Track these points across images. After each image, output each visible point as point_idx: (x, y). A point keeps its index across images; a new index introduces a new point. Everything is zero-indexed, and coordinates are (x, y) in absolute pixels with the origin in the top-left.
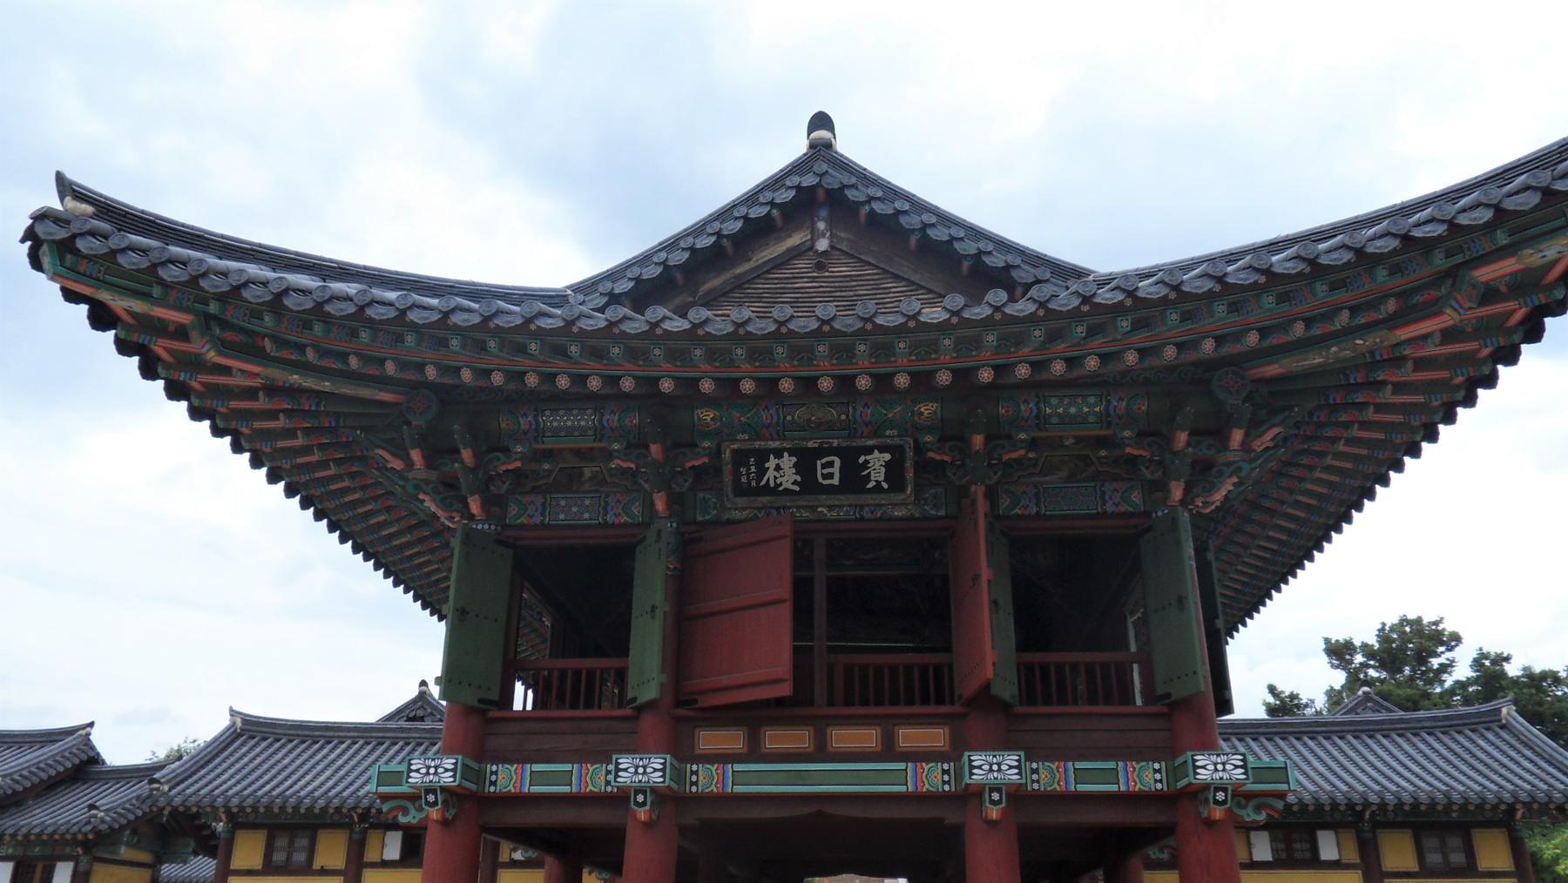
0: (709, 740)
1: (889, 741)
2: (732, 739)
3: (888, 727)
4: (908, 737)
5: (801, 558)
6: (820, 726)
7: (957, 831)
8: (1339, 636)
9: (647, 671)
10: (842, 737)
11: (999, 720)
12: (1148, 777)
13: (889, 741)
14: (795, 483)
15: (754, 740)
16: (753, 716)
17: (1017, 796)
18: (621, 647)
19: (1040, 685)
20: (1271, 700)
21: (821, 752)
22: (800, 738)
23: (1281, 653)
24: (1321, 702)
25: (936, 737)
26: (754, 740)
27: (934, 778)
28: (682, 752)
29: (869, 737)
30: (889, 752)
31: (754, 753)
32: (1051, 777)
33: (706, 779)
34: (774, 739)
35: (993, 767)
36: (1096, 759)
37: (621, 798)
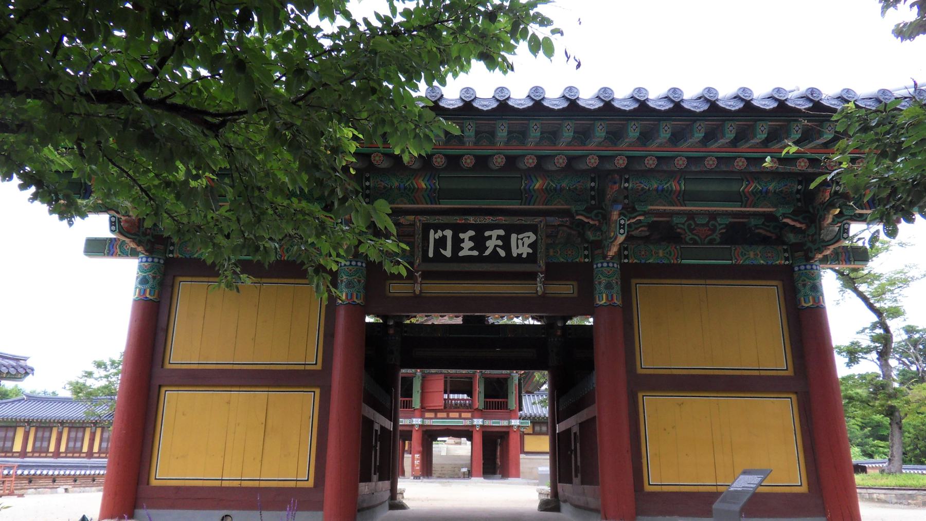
0: (427, 415)
1: (460, 416)
2: (432, 415)
3: (460, 412)
4: (464, 415)
5: (445, 382)
6: (448, 412)
8: (98, 359)
9: (416, 402)
10: (451, 415)
11: (481, 413)
12: (505, 423)
13: (460, 416)
16: (436, 411)
17: (482, 426)
18: (506, 396)
19: (487, 406)
21: (448, 418)
22: (444, 415)
23: (317, 8)
24: (474, 62)
27: (468, 423)
28: (422, 417)
29: (457, 415)
30: (460, 418)
31: (436, 418)
32: (488, 423)
33: (428, 422)
34: (439, 415)
35: (478, 422)
36: (694, 265)
37: (413, 425)
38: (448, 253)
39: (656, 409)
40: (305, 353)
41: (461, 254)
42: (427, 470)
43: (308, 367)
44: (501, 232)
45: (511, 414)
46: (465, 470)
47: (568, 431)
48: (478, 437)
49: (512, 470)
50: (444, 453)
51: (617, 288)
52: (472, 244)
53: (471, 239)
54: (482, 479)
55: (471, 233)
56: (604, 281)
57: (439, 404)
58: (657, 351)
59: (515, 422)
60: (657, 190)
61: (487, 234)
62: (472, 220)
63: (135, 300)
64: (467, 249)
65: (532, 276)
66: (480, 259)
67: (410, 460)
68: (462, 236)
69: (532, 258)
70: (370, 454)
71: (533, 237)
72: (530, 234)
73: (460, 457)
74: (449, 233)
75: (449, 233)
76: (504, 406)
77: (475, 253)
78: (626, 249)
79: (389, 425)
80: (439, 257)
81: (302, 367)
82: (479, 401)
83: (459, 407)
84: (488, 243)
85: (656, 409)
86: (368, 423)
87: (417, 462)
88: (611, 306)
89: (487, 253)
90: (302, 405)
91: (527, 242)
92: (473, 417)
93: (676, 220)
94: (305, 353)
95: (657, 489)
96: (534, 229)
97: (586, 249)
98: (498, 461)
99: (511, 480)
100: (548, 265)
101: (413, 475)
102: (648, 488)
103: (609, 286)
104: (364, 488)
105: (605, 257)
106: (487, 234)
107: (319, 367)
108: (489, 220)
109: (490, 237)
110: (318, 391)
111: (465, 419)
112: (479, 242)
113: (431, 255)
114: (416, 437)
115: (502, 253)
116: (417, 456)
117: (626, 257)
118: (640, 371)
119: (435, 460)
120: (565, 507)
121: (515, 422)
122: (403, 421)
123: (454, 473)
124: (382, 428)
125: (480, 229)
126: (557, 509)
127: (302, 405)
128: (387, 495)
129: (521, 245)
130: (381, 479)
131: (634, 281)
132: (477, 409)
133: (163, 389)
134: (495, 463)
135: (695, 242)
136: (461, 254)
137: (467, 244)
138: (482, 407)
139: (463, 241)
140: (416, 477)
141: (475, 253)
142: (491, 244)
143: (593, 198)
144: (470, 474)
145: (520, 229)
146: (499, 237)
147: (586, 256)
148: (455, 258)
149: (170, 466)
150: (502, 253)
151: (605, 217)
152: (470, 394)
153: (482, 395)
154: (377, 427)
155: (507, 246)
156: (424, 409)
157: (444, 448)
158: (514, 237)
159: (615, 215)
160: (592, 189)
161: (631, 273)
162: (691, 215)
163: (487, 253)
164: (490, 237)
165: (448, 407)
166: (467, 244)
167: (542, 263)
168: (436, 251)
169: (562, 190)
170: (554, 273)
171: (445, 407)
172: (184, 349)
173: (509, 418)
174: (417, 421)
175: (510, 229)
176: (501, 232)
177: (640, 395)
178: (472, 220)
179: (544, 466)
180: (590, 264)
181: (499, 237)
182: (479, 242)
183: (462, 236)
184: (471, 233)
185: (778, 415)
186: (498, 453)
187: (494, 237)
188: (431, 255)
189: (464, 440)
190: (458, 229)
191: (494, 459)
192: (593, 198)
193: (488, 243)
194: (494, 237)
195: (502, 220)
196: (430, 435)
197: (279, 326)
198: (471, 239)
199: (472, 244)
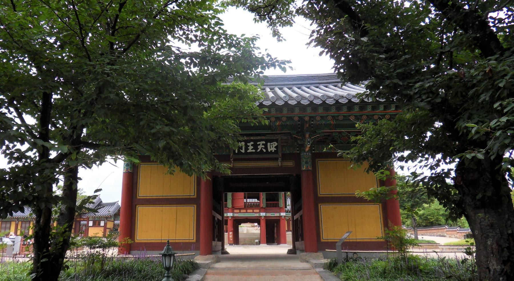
0: (236, 211)
2: (238, 211)
3: (253, 210)
4: (255, 211)
6: (247, 210)
7: (260, 220)
10: (248, 211)
12: (278, 215)
14: (318, 27)
15: (240, 211)
16: (240, 209)
18: (278, 200)
19: (268, 206)
20: (366, 164)
21: (247, 212)
22: (245, 211)
25: (258, 211)
26: (240, 211)
27: (257, 215)
28: (233, 212)
29: (251, 211)
30: (253, 212)
31: (240, 212)
32: (269, 215)
33: (236, 215)
34: (242, 211)
35: (263, 214)
38: (243, 151)
39: (325, 209)
40: (190, 191)
41: (248, 151)
42: (236, 241)
43: (191, 197)
44: (264, 142)
45: (281, 210)
46: (257, 241)
47: (297, 219)
48: (263, 223)
49: (282, 240)
50: (245, 232)
51: (310, 163)
52: (252, 147)
53: (252, 145)
54: (266, 245)
55: (252, 143)
56: (305, 161)
57: (242, 205)
58: (325, 189)
59: (283, 214)
60: (324, 124)
61: (258, 143)
62: (252, 138)
63: (124, 173)
64: (251, 149)
65: (276, 159)
66: (256, 153)
67: (228, 236)
68: (248, 144)
69: (276, 152)
70: (214, 231)
71: (276, 144)
72: (275, 143)
73: (254, 234)
74: (243, 143)
75: (243, 143)
76: (277, 206)
77: (254, 151)
78: (313, 147)
79: (220, 218)
80: (240, 153)
81: (189, 197)
82: (263, 204)
83: (252, 206)
84: (259, 147)
85: (325, 209)
86: (214, 217)
87: (231, 236)
88: (308, 171)
89: (259, 151)
90: (190, 211)
91: (274, 146)
92: (260, 212)
93: (334, 134)
94: (190, 191)
95: (326, 241)
96: (276, 141)
97: (298, 147)
98: (275, 236)
99: (281, 245)
100: (283, 154)
101: (229, 243)
102: (322, 240)
103: (307, 163)
104: (214, 243)
105: (305, 151)
106: (258, 143)
107: (195, 196)
108: (259, 138)
109: (259, 144)
110: (195, 206)
111: (256, 213)
112: (255, 146)
113: (236, 152)
114: (230, 223)
115: (264, 151)
116: (231, 233)
117: (314, 150)
118: (319, 196)
119: (240, 236)
120: (298, 252)
121: (283, 214)
122: (225, 215)
123: (251, 242)
124: (218, 219)
125: (255, 141)
126: (295, 253)
127: (190, 211)
128: (220, 248)
129: (272, 147)
130: (218, 241)
131: (317, 160)
132: (262, 208)
133: (137, 206)
134: (274, 237)
135: (342, 143)
136: (248, 151)
137: (251, 147)
138: (264, 206)
139: (249, 146)
140: (230, 244)
141: (254, 151)
142: (260, 147)
143: (299, 128)
144: (259, 243)
145: (271, 141)
146: (263, 144)
147: (298, 150)
148: (246, 153)
149: (142, 235)
150: (264, 151)
151: (304, 136)
152: (258, 199)
153: (265, 200)
154: (216, 219)
155: (266, 148)
156: (234, 208)
157: (245, 229)
158: (269, 144)
159: (307, 136)
160: (299, 124)
161: (316, 156)
162: (340, 133)
163: (259, 151)
164: (259, 144)
165: (247, 206)
166: (251, 147)
167: (280, 154)
168: (239, 150)
169: (287, 125)
170: (285, 157)
171: (245, 207)
172: (144, 191)
173: (280, 212)
174: (230, 215)
175: (267, 141)
176: (264, 142)
177: (319, 205)
178: (252, 138)
179: (289, 235)
180: (300, 153)
181: (263, 144)
182: (255, 146)
183: (248, 144)
184: (252, 143)
185: (375, 211)
186: (275, 231)
187: (261, 144)
188: (236, 152)
189: (256, 224)
190: (246, 142)
191: (271, 235)
192: (299, 128)
193: (259, 147)
194: (261, 144)
195: (264, 138)
196: (238, 222)
197: (183, 185)
198: (252, 145)
199: (252, 147)
